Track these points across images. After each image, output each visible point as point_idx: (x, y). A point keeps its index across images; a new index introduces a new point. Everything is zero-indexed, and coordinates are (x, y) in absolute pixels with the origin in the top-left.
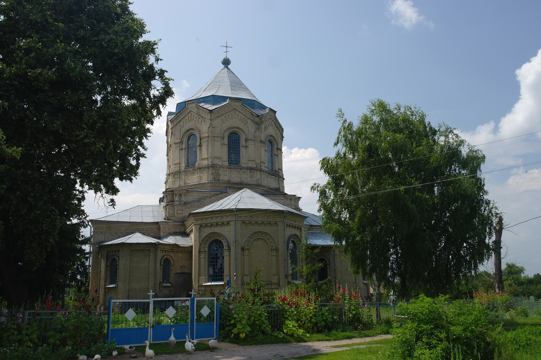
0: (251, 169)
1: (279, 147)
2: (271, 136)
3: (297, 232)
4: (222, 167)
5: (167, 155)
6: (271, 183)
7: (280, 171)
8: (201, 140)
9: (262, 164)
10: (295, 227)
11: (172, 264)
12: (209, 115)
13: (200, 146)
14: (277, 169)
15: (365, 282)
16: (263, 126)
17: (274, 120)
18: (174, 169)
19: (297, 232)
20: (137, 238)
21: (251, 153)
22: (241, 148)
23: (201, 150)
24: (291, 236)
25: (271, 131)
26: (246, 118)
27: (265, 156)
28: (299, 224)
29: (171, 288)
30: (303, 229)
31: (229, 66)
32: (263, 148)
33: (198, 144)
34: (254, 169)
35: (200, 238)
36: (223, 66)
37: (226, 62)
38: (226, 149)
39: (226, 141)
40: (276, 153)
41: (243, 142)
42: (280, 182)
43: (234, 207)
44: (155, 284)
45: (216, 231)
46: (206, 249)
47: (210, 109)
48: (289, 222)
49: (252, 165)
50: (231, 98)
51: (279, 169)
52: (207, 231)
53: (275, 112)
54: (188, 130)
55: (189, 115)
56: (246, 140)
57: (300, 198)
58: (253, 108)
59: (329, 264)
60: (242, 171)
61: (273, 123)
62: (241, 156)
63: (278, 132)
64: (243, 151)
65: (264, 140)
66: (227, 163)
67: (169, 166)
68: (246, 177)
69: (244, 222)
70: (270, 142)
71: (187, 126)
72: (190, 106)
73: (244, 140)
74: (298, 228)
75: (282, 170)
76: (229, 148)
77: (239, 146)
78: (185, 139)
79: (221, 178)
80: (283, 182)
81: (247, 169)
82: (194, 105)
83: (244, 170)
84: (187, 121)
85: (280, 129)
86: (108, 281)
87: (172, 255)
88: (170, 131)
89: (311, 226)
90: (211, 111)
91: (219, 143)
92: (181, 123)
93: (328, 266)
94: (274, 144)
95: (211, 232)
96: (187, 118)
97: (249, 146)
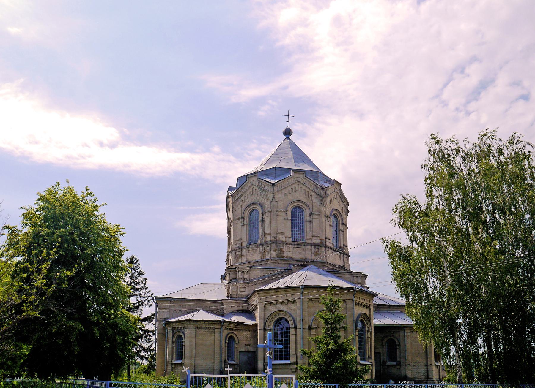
0: (315, 245)
1: (344, 222)
2: (336, 210)
3: (366, 311)
4: (286, 243)
5: (228, 232)
6: (335, 259)
7: (345, 247)
8: (263, 215)
9: (327, 240)
10: (364, 306)
11: (237, 341)
12: (272, 189)
13: (263, 221)
14: (342, 246)
15: (437, 364)
16: (328, 199)
17: (339, 194)
18: (235, 246)
19: (366, 311)
20: (201, 315)
21: (319, 228)
22: (305, 223)
23: (263, 227)
24: (359, 316)
25: (337, 205)
26: (310, 191)
27: (330, 232)
28: (368, 303)
29: (236, 366)
30: (372, 308)
31: (291, 137)
32: (328, 224)
33: (260, 218)
34: (319, 246)
35: (264, 316)
36: (285, 137)
37: (288, 133)
38: (289, 223)
39: (289, 216)
40: (341, 228)
41: (307, 218)
42: (345, 259)
43: (301, 284)
44: (221, 362)
45: (281, 309)
46: (272, 327)
47: (273, 182)
48: (358, 300)
49: (316, 240)
50: (294, 170)
51: (344, 245)
52: (272, 309)
53: (341, 184)
54: (249, 205)
55: (251, 189)
56: (311, 215)
57: (366, 276)
58: (318, 180)
59: (399, 345)
60: (306, 247)
61: (338, 196)
62: (305, 232)
63: (343, 206)
64: (307, 226)
65: (328, 213)
66: (290, 240)
67: (230, 243)
68: (309, 254)
69: (311, 300)
70: (336, 217)
71: (249, 200)
72: (251, 180)
73: (308, 215)
74: (367, 306)
75: (347, 247)
76: (292, 223)
77: (303, 221)
78: (247, 215)
79: (284, 255)
80: (348, 259)
81: (312, 245)
82: (255, 179)
83: (309, 247)
84: (249, 195)
85: (347, 204)
86: (174, 358)
87: (236, 332)
88: (231, 206)
89: (379, 305)
90: (273, 184)
91: (282, 218)
92: (243, 198)
93: (398, 347)
94: (339, 220)
95: (276, 310)
96: (248, 192)
97: (314, 220)
